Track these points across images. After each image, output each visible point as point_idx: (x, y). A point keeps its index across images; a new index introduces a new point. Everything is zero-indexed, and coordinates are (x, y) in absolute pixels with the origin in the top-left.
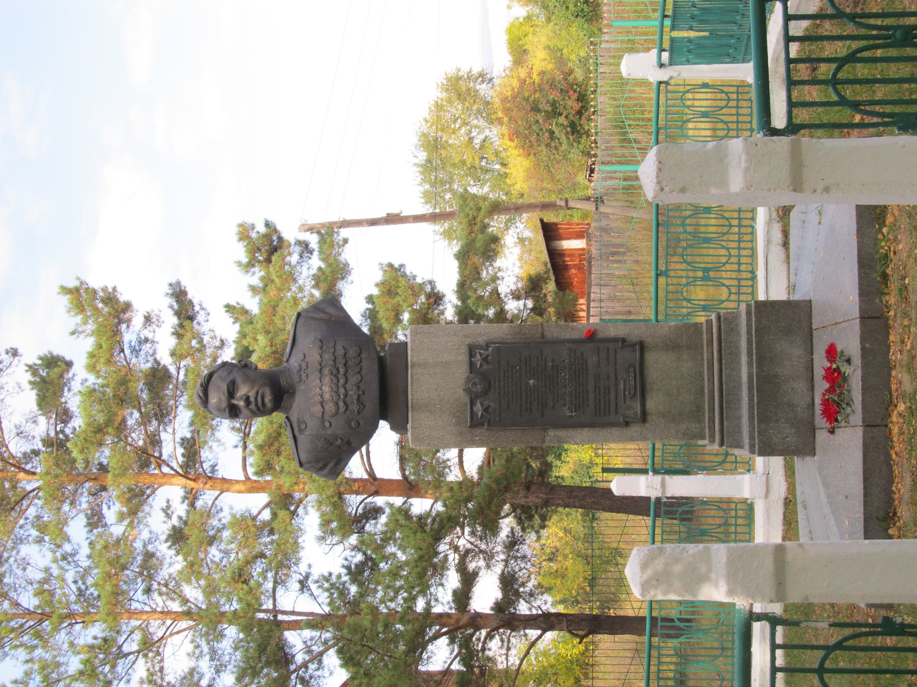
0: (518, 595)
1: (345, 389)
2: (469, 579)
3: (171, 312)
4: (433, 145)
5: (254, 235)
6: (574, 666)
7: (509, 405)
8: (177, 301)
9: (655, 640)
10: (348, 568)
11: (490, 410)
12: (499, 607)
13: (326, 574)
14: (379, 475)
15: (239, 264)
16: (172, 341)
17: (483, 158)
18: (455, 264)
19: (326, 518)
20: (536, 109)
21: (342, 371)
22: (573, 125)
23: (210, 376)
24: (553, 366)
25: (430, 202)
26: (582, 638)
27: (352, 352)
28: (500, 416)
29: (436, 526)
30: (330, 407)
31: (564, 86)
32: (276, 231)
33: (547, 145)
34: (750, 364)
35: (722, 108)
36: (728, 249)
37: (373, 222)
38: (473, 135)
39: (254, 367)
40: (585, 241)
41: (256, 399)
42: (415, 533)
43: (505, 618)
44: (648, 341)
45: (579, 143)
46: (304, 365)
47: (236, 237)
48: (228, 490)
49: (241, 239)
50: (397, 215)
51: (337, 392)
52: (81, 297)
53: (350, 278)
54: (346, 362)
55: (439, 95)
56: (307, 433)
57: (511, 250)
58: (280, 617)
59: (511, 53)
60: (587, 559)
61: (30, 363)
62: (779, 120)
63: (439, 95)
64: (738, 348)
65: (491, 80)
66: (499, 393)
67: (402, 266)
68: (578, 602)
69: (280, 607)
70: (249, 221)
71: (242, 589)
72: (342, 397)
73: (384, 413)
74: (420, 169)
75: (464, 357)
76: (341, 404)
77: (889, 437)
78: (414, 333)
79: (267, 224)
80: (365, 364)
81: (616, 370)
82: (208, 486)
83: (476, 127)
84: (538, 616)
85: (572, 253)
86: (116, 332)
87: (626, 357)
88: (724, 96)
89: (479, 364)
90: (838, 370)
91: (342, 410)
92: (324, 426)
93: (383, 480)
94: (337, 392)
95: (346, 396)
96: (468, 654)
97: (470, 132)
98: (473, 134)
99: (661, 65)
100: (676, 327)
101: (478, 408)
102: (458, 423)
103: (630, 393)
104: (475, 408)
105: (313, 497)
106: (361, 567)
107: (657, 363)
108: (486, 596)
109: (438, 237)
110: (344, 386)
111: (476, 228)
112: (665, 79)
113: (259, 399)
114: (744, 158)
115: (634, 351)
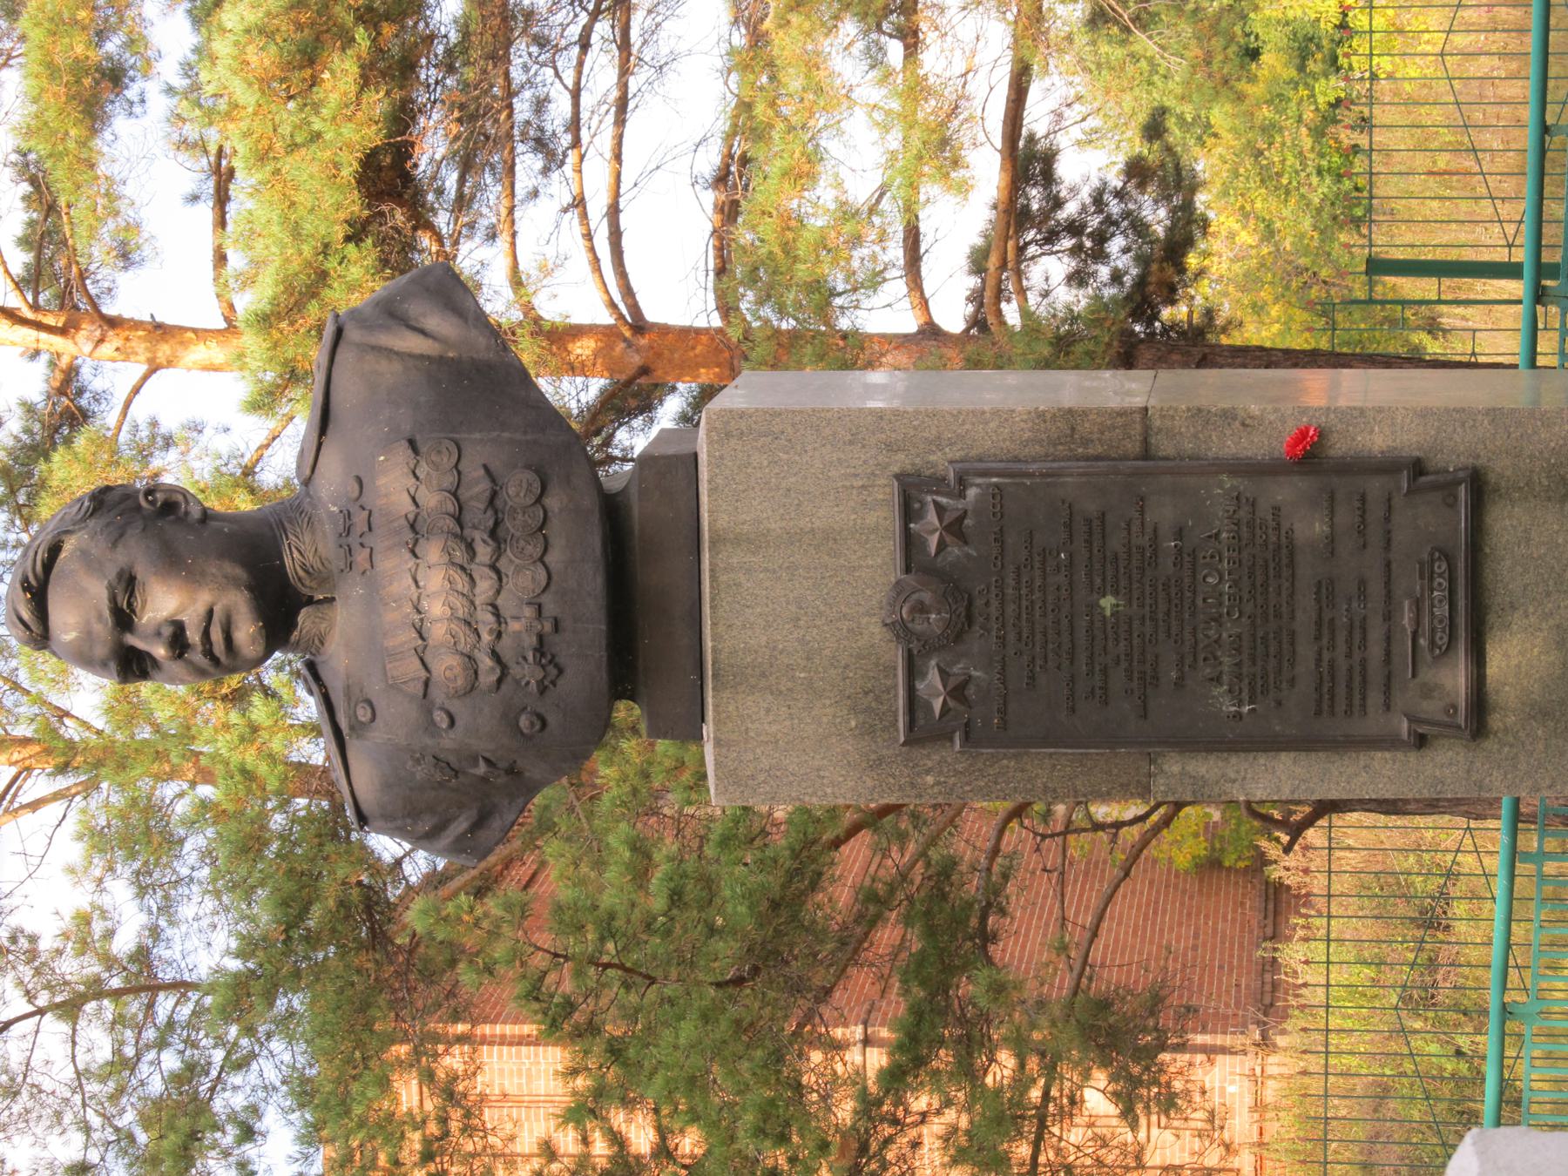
1: (497, 613)
7: (1032, 678)
11: (971, 691)
14: (652, 315)
24: (1179, 551)
28: (1003, 712)
39: (196, 513)
41: (206, 634)
44: (1500, 468)
54: (497, 523)
56: (378, 734)
66: (1002, 640)
71: (227, 727)
72: (486, 638)
75: (887, 518)
76: (486, 662)
81: (1388, 565)
82: (107, 349)
87: (1423, 522)
89: (933, 542)
91: (488, 678)
92: (433, 723)
93: (664, 330)
101: (932, 684)
102: (867, 731)
103: (1433, 643)
104: (920, 686)
113: (217, 635)
115: (1452, 504)
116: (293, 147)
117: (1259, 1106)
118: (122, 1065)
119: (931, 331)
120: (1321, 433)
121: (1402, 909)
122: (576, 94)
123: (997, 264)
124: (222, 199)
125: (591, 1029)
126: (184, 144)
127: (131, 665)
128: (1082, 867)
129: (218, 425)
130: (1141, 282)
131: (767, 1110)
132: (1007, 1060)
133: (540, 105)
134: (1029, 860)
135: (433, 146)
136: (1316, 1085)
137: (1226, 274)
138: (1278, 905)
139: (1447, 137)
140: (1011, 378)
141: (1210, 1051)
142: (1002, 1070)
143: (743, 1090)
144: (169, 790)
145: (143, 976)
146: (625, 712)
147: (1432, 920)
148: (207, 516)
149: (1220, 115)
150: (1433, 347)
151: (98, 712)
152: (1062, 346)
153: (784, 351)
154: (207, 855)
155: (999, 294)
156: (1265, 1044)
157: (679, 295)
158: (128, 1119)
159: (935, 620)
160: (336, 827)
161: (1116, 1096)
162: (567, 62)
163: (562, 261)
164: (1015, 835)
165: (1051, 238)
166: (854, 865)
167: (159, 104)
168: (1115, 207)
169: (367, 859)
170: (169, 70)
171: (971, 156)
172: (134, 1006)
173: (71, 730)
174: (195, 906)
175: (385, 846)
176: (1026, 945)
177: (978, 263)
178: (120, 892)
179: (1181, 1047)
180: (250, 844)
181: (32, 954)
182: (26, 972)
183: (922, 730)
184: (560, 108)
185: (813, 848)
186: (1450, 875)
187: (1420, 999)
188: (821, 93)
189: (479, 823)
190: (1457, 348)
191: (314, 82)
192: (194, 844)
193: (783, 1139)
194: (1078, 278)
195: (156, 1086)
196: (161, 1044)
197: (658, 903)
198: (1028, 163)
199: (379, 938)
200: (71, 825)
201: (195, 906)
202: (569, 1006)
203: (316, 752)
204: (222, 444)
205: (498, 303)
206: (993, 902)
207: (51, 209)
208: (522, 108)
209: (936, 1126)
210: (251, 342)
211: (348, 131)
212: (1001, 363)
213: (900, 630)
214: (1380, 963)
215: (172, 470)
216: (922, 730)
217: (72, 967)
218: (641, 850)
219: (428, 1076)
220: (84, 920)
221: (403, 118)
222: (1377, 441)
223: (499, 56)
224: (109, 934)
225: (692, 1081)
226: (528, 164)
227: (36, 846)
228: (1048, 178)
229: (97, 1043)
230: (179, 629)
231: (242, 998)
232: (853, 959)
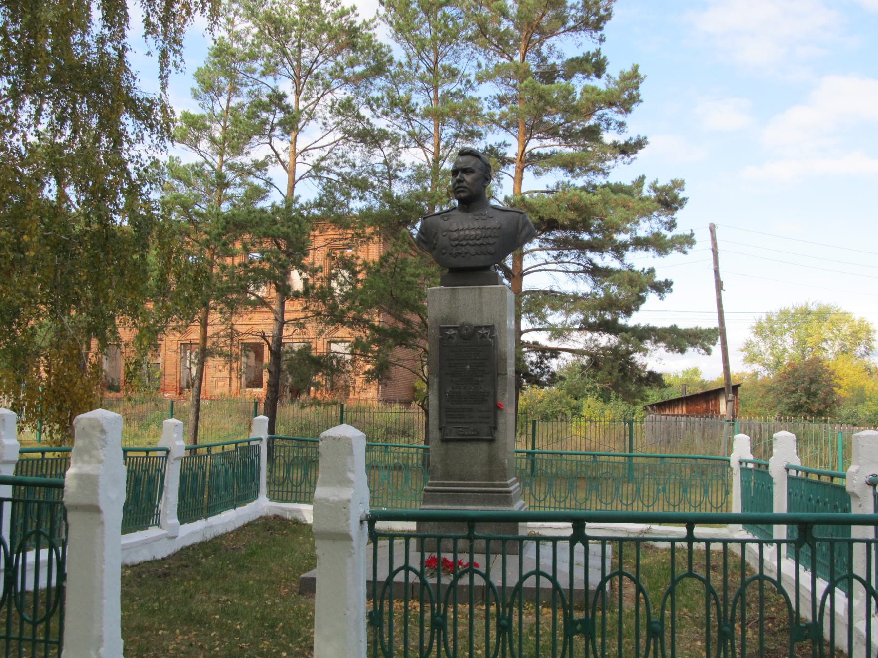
3: (627, 139)
4: (822, 315)
5: (676, 191)
8: (635, 143)
15: (656, 182)
18: (667, 325)
20: (812, 381)
21: (478, 242)
22: (801, 406)
27: (491, 249)
30: (455, 235)
31: (829, 401)
33: (786, 389)
35: (711, 503)
36: (545, 499)
37: (717, 272)
45: (789, 410)
46: (484, 217)
47: (673, 179)
49: (672, 182)
51: (464, 239)
52: (632, 79)
56: (441, 221)
61: (602, 51)
62: (380, 525)
65: (868, 354)
67: (671, 291)
70: (686, 187)
76: (456, 242)
79: (684, 199)
80: (482, 257)
85: (717, 405)
86: (611, 104)
88: (719, 505)
93: (522, 280)
94: (464, 239)
95: (462, 245)
98: (829, 342)
99: (741, 462)
100: (504, 464)
109: (757, 319)
110: (468, 244)
112: (731, 464)
114: (336, 498)
116: (558, 206)
117: (367, 399)
118: (374, 173)
119: (522, 333)
120: (502, 410)
121: (407, 427)
122: (569, 262)
123: (536, 347)
124: (547, 192)
125: (382, 266)
126: (558, 184)
127: (455, 172)
128: (413, 365)
129: (502, 189)
130: (531, 375)
131: (367, 301)
132: (376, 349)
133: (567, 256)
134: (416, 353)
135: (558, 234)
136: (371, 410)
137: (531, 394)
138: (407, 403)
139: (560, 437)
140: (513, 350)
141: (378, 389)
142: (375, 348)
143: (370, 296)
144: (430, 183)
145: (392, 177)
146: (446, 271)
147: (404, 433)
148: (485, 187)
149: (563, 392)
150: (518, 434)
152: (519, 359)
153: (518, 304)
154: (417, 190)
155: (529, 347)
156: (379, 401)
157: (529, 283)
158: (364, 175)
160: (421, 214)
161: (369, 370)
162: (575, 260)
163: (536, 259)
164: (421, 350)
165: (540, 357)
166: (415, 319)
167: (566, 180)
168: (546, 370)
169: (416, 222)
170: (573, 182)
171: (556, 341)
172: (386, 176)
173: (441, 162)
174: (406, 187)
175: (418, 225)
176: (399, 352)
177: (535, 343)
178: (409, 172)
179: (379, 384)
180: (419, 198)
181: (396, 155)
182: (393, 154)
183: (443, 330)
184: (566, 260)
185: (419, 310)
186: (413, 437)
187: (389, 431)
188: (568, 312)
189: (424, 242)
190: (518, 439)
191: (571, 210)
192: (418, 187)
193: (361, 304)
194: (532, 363)
195: (370, 180)
196: (379, 181)
197: (407, 279)
198: (555, 353)
199: (400, 224)
200: (422, 163)
201: (406, 187)
202: (387, 261)
203: (437, 210)
204: (499, 192)
205: (527, 247)
206: (408, 346)
207: (545, 158)
208: (566, 252)
209: (363, 335)
210: (519, 197)
211: (561, 217)
212: (516, 347)
213: (463, 325)
214: (395, 423)
215: (494, 182)
216: (443, 330)
217: (394, 162)
218: (418, 276)
219: (373, 234)
220: (404, 165)
221: (564, 228)
222: (501, 420)
223: (576, 247)
224: (400, 170)
225: (372, 286)
226: (555, 253)
227: (418, 156)
228: (552, 357)
229: (379, 169)
230: (462, 182)
231: (388, 196)
232: (396, 318)
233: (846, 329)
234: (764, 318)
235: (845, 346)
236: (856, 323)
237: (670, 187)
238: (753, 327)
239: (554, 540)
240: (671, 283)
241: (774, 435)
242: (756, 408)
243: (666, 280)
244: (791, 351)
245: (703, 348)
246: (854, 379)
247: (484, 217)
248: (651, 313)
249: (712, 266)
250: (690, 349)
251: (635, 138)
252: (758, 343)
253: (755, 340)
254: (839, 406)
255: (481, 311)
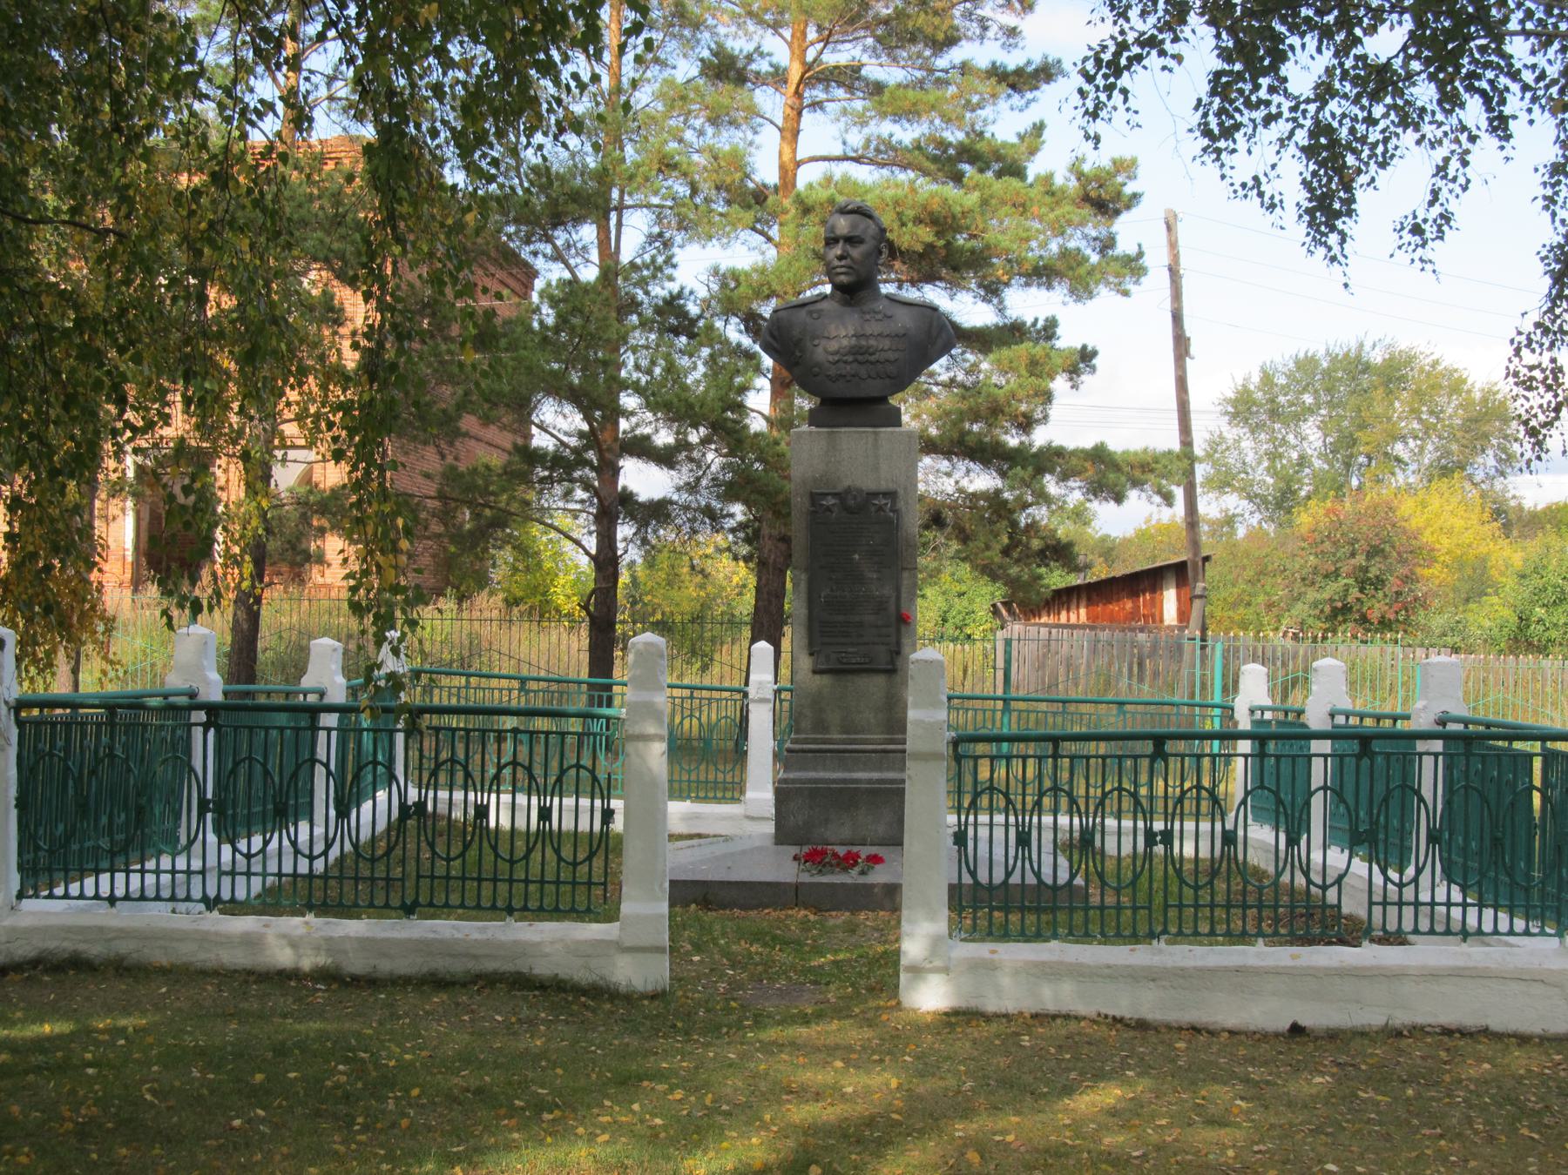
0: (643, 524)
2: (665, 458)
4: (1393, 374)
5: (1120, 179)
6: (539, 597)
8: (1036, 70)
9: (584, 687)
10: (680, 295)
12: (627, 498)
13: (675, 261)
16: (983, 63)
17: (1370, 459)
18: (1088, 443)
19: (742, 278)
22: (1346, 609)
23: (870, 217)
25: (1298, 368)
26: (585, 607)
27: (891, 369)
29: (729, 425)
32: (1128, 207)
34: (870, 781)
37: (1177, 318)
38: (1410, 441)
40: (1175, 623)
42: (721, 399)
43: (614, 506)
47: (1117, 155)
48: (783, 138)
49: (1114, 162)
50: (1187, 353)
53: (1072, 304)
55: (1478, 386)
56: (808, 320)
57: (1214, 504)
58: (613, 216)
59: (1549, 508)
60: (698, 619)
63: (1478, 386)
64: (888, 769)
65: (1503, 474)
67: (1093, 369)
68: (634, 603)
69: (626, 214)
70: (1140, 172)
73: (823, 402)
74: (1352, 354)
75: (884, 486)
77: (785, 907)
78: (910, 434)
79: (1135, 197)
82: (789, 111)
83: (1422, 449)
84: (613, 548)
85: (1157, 605)
90: (856, 863)
96: (562, 464)
97: (1415, 438)
98: (1411, 443)
99: (1252, 712)
101: (831, 501)
105: (772, 252)
106: (682, 313)
107: (874, 685)
108: (643, 480)
111: (1137, 473)
151: (1208, 436)
159: (851, 502)
183: (814, 498)
213: (848, 490)
216: (814, 498)
233: (1451, 408)
234: (1256, 378)
235: (1449, 453)
236: (1477, 395)
237: (1108, 173)
238: (1228, 401)
239: (1135, 757)
240: (1094, 353)
241: (1315, 664)
242: (1234, 606)
243: (1084, 347)
244: (1317, 463)
245: (1159, 492)
246: (1468, 537)
247: (879, 316)
248: (1070, 421)
249: (1167, 305)
250: (1133, 494)
251: (1037, 61)
252: (1238, 441)
253: (1231, 433)
254: (1425, 607)
255: (876, 469)
